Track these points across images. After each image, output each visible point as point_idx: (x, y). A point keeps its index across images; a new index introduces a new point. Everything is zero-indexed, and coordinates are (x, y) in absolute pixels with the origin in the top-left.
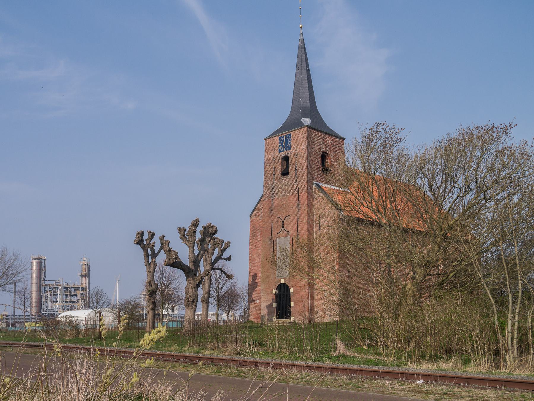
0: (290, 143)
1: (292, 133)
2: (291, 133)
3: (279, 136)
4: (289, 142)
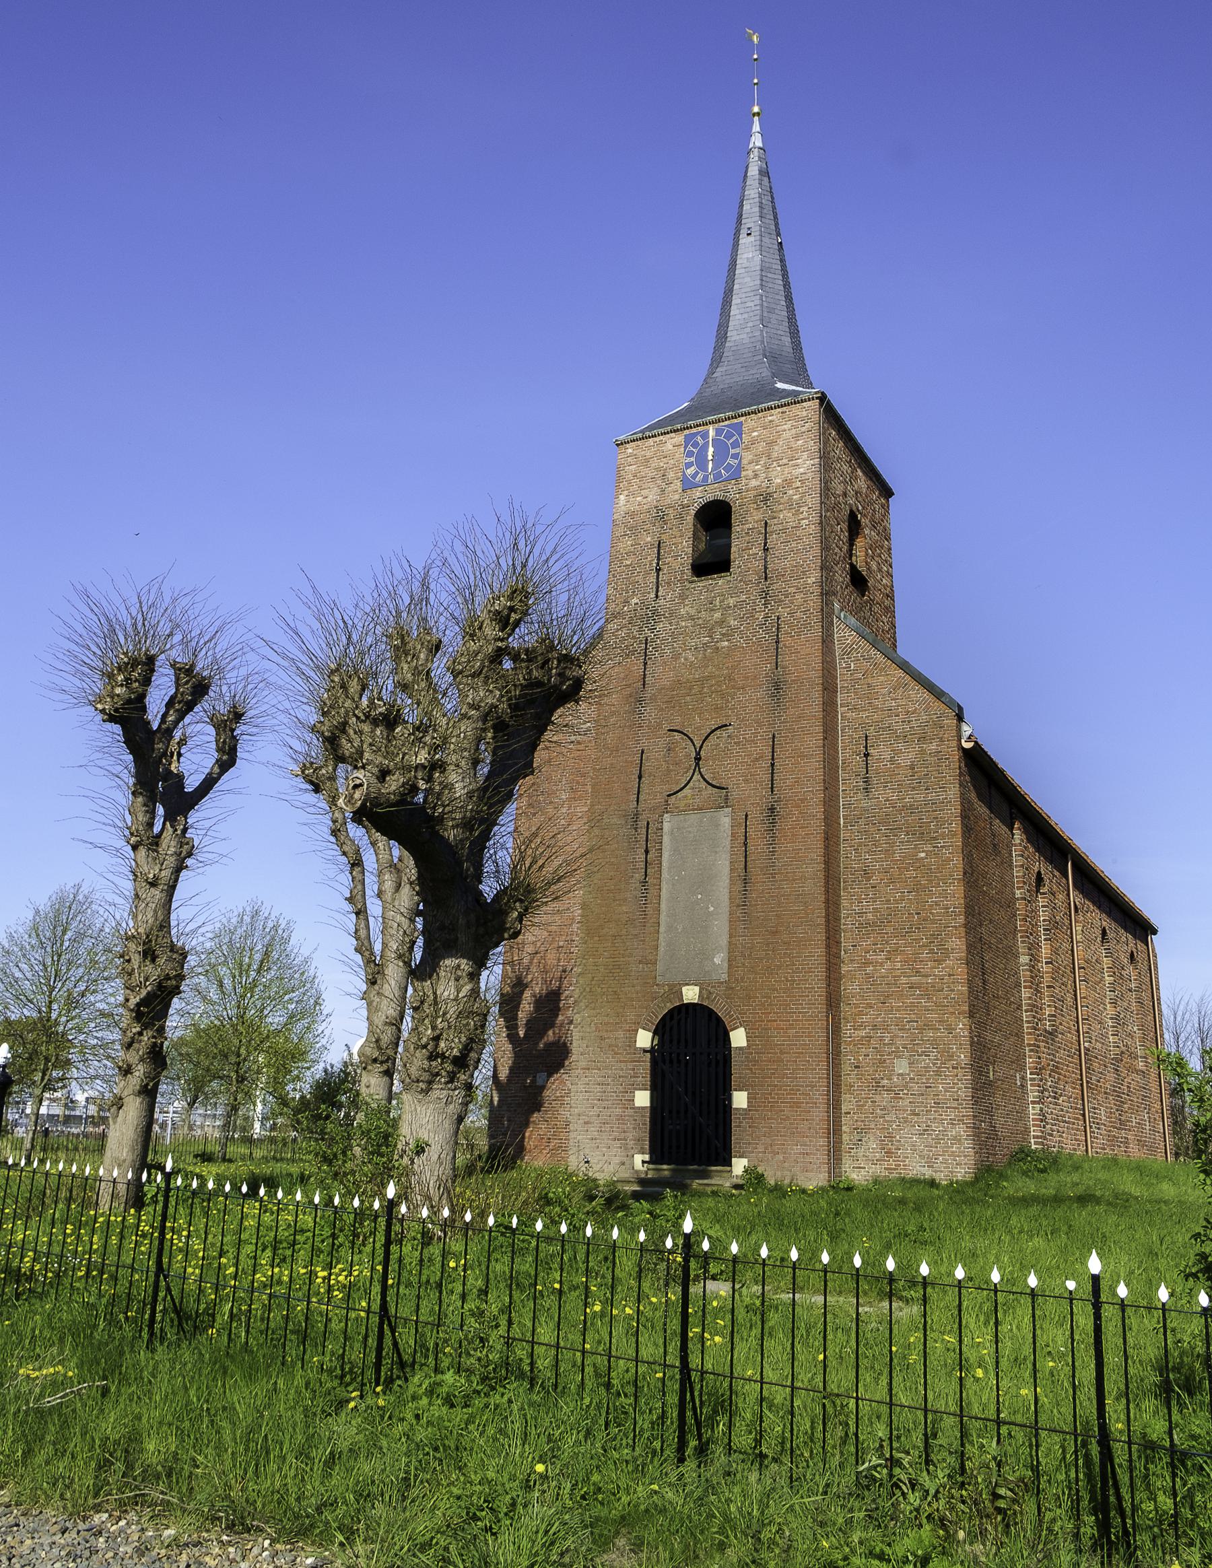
0: (735, 456)
1: (748, 423)
2: (742, 419)
3: (687, 432)
4: (732, 451)
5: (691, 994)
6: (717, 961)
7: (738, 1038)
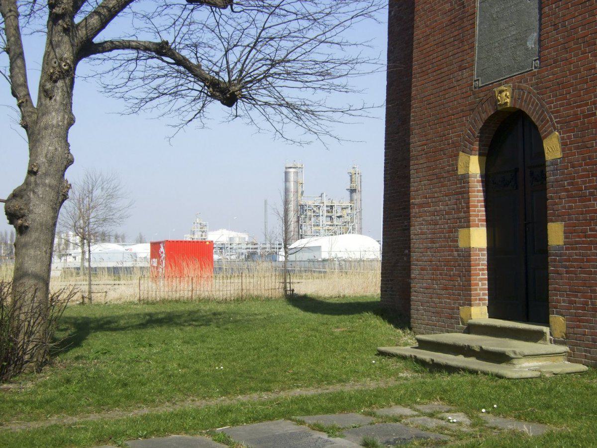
7: (552, 149)
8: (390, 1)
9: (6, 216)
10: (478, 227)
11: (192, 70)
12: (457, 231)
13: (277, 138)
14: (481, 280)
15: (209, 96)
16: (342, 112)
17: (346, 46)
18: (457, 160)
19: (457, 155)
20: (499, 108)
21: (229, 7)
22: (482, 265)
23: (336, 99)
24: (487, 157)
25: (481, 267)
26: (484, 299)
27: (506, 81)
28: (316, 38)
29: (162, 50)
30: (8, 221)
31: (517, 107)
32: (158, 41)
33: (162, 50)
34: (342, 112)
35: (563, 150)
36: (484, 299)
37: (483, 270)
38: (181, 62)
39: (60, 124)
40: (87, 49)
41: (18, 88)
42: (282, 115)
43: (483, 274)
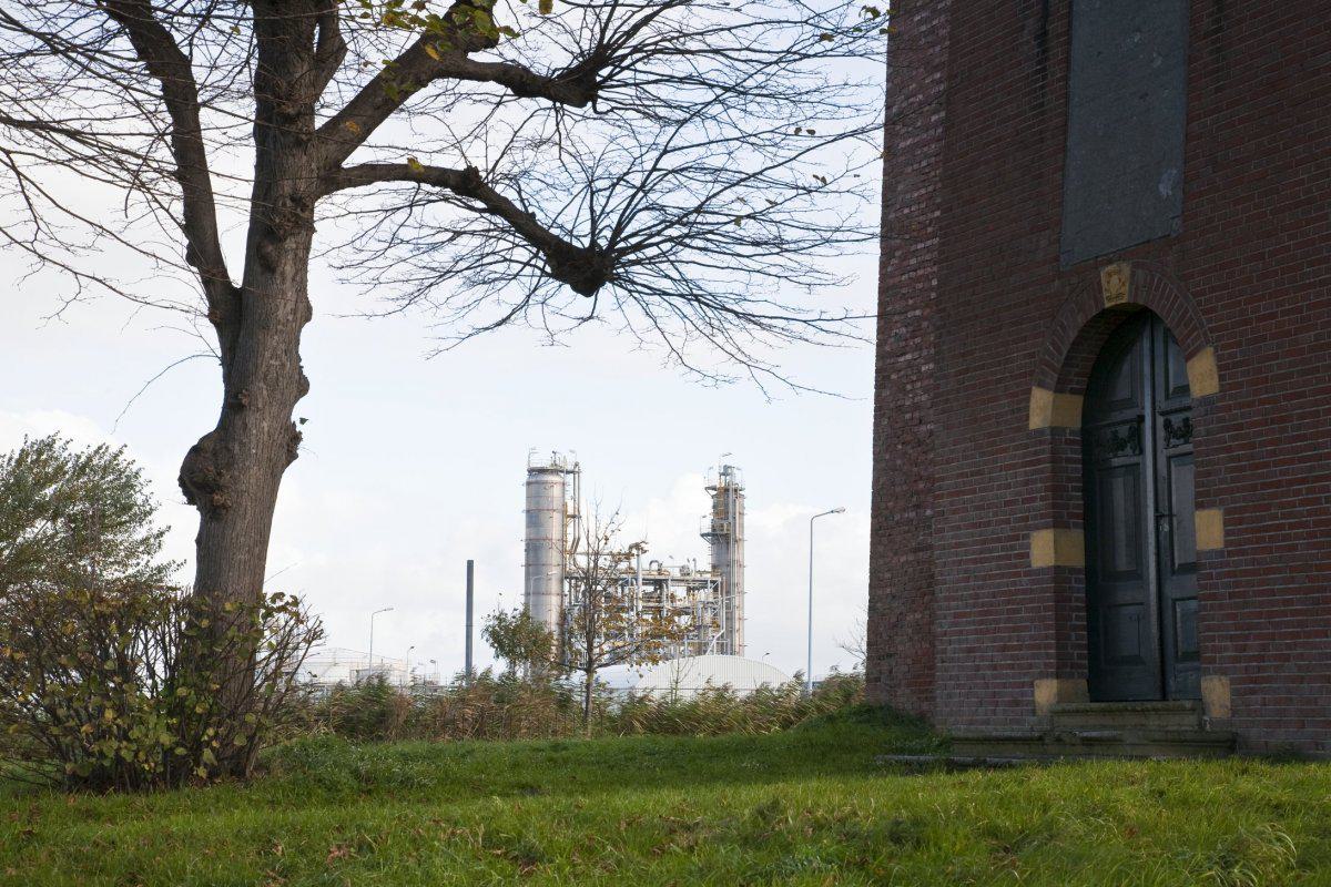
5: (1116, 286)
6: (1164, 190)
8: (892, 4)
9: (180, 489)
10: (1069, 528)
11: (524, 224)
12: (1026, 537)
13: (671, 364)
14: (1075, 628)
15: (548, 275)
16: (805, 322)
17: (230, 210)
18: (1028, 400)
19: (1029, 392)
20: (1108, 305)
21: (590, 104)
22: (1077, 599)
23: (790, 296)
24: (1085, 396)
25: (1074, 604)
26: (1080, 666)
27: (1121, 256)
28: (761, 173)
29: (466, 184)
30: (185, 499)
31: (1141, 302)
32: (461, 167)
33: (466, 184)
34: (805, 322)
35: (1221, 378)
36: (1080, 666)
37: (1078, 609)
38: (498, 206)
39: (290, 318)
40: (335, 179)
41: (203, 253)
42: (685, 320)
43: (1078, 618)
